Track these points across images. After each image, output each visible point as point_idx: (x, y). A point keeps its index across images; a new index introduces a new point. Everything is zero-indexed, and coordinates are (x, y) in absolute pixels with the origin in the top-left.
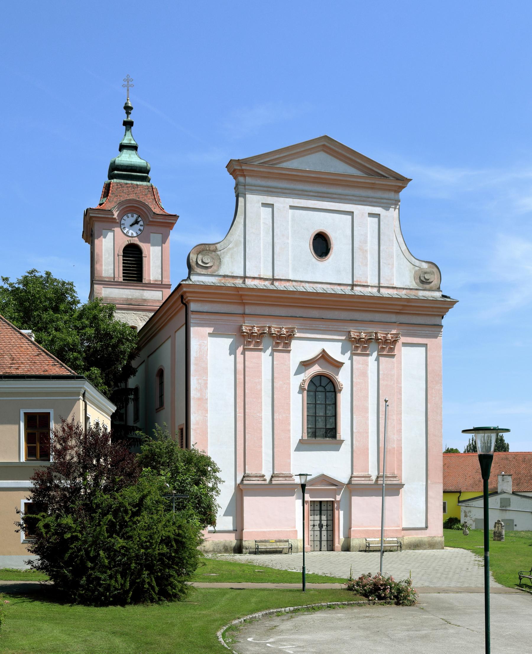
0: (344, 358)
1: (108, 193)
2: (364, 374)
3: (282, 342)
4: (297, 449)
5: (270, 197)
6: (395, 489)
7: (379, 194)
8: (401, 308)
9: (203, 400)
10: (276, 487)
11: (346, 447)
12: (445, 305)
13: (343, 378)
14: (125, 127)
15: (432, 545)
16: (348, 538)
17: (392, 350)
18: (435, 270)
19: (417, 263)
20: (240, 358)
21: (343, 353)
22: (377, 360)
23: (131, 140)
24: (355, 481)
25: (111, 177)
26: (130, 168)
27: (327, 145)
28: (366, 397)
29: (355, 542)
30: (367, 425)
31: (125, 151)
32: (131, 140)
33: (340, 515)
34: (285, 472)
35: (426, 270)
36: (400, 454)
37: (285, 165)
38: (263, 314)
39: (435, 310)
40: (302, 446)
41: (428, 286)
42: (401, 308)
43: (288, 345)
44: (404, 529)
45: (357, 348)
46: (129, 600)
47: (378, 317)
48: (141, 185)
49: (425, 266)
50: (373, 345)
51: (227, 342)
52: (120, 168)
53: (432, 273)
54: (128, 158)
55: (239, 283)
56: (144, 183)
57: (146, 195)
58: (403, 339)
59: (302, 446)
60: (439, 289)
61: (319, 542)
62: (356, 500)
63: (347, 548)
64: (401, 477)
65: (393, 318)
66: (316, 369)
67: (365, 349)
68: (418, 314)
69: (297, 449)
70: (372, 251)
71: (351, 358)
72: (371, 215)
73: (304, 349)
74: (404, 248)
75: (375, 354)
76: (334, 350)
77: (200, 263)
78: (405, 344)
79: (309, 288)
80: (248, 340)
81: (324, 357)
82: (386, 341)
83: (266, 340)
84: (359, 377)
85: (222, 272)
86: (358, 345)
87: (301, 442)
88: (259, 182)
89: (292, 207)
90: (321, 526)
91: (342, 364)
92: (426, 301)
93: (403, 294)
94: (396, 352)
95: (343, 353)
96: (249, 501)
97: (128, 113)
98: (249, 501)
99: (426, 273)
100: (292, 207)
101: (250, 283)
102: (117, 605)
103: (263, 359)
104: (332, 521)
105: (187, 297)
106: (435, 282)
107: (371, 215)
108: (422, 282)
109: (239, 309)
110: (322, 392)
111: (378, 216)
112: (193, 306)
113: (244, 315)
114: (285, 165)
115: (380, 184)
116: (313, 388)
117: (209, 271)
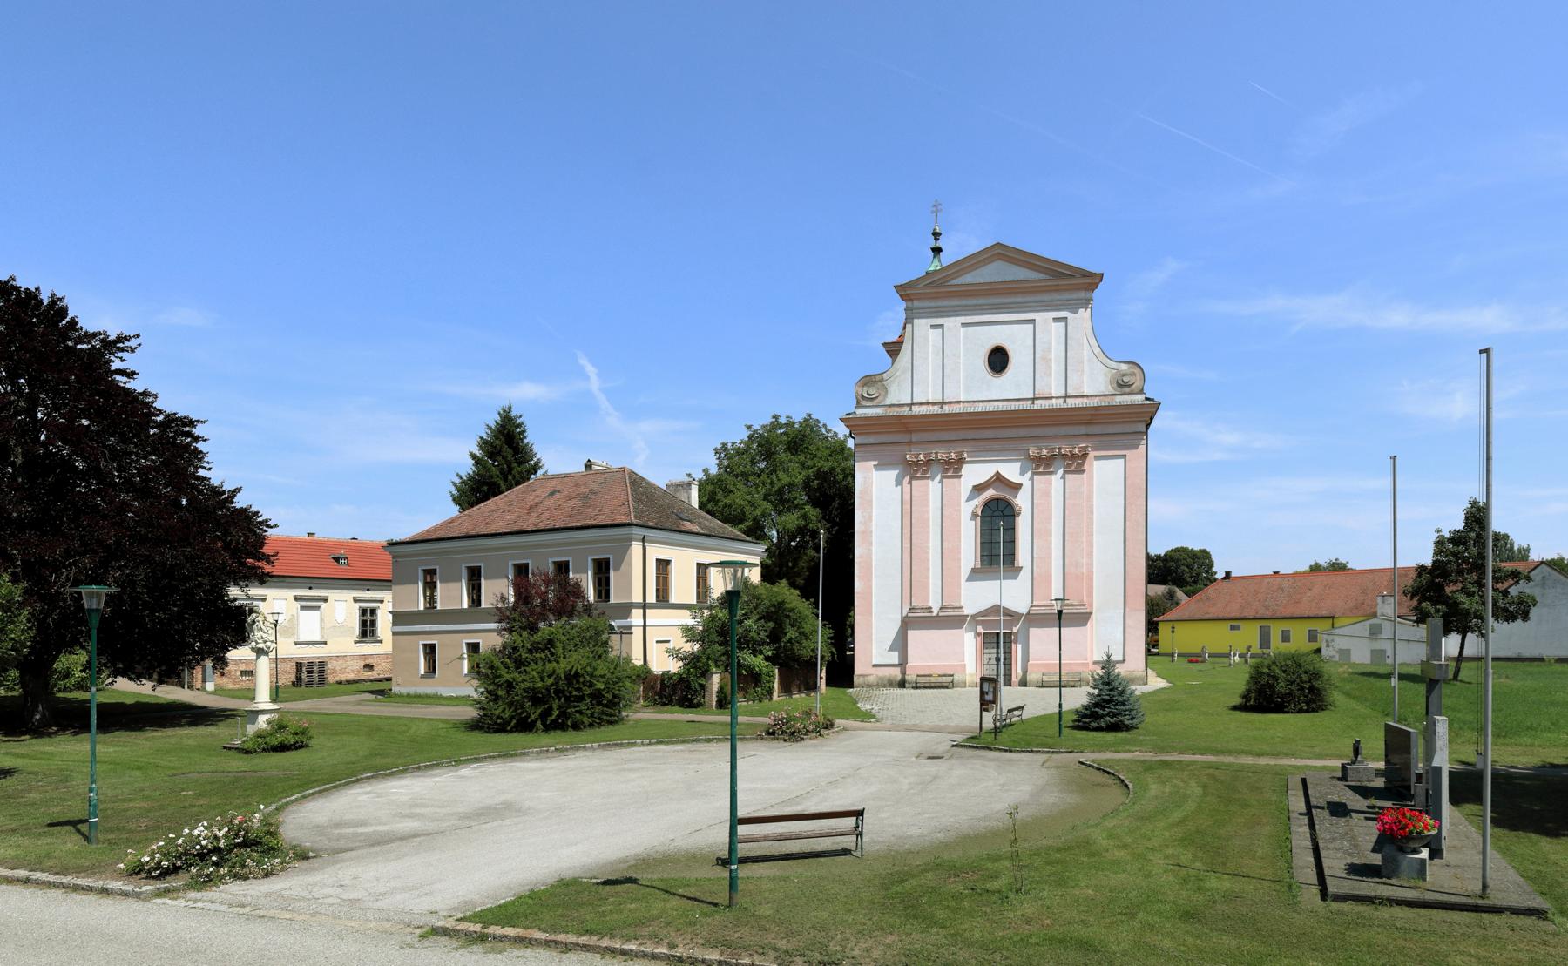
0: (1024, 480)
2: (1047, 494)
3: (953, 467)
4: (969, 579)
6: (1083, 619)
7: (1066, 296)
9: (867, 533)
10: (950, 620)
11: (1025, 575)
12: (1146, 415)
13: (1022, 501)
16: (1025, 672)
17: (1081, 465)
18: (1137, 370)
19: (1114, 365)
20: (907, 487)
21: (1022, 473)
22: (1063, 477)
24: (1035, 611)
27: (1000, 252)
28: (1049, 519)
29: (1031, 677)
30: (1049, 548)
33: (1018, 649)
34: (955, 603)
36: (1091, 579)
37: (955, 282)
38: (929, 441)
40: (975, 574)
43: (959, 469)
45: (1038, 466)
47: (1063, 430)
49: (1124, 367)
50: (1058, 462)
51: (892, 474)
53: (1133, 374)
55: (905, 411)
58: (1092, 454)
59: (975, 574)
60: (1141, 392)
62: (1034, 632)
63: (1023, 683)
64: (1091, 605)
65: (1083, 430)
66: (990, 493)
67: (1048, 466)
68: (1121, 423)
69: (969, 579)
70: (1059, 358)
71: (1032, 479)
72: (1056, 320)
73: (976, 472)
74: (1097, 350)
75: (1061, 472)
76: (1011, 470)
78: (1097, 458)
79: (980, 408)
80: (917, 469)
81: (998, 479)
82: (1072, 457)
83: (935, 468)
84: (1041, 499)
85: (888, 402)
86: (1041, 464)
87: (974, 570)
88: (927, 304)
89: (964, 325)
90: (998, 660)
91: (1020, 485)
92: (1132, 406)
93: (1092, 403)
94: (1086, 467)
95: (1022, 473)
96: (912, 635)
98: (912, 635)
100: (964, 325)
101: (917, 410)
102: (220, 499)
103: (932, 488)
104: (1008, 653)
106: (1138, 384)
107: (1056, 320)
108: (1120, 386)
109: (906, 438)
110: (998, 516)
111: (1065, 319)
113: (910, 443)
114: (955, 282)
115: (1065, 285)
116: (989, 512)
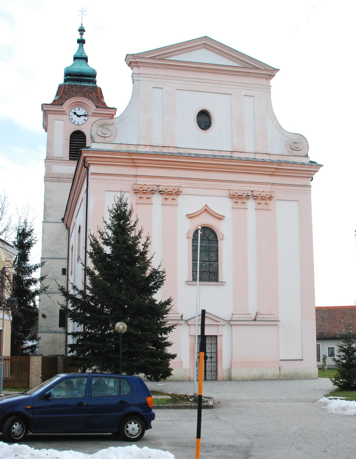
8: (273, 170)
13: (224, 230)
14: (78, 44)
15: (307, 377)
27: (206, 43)
35: (295, 141)
39: (303, 172)
41: (295, 153)
42: (273, 170)
44: (281, 360)
54: (80, 67)
56: (91, 85)
73: (189, 203)
97: (82, 34)
99: (295, 143)
105: (88, 161)
112: (92, 169)
117: (108, 140)
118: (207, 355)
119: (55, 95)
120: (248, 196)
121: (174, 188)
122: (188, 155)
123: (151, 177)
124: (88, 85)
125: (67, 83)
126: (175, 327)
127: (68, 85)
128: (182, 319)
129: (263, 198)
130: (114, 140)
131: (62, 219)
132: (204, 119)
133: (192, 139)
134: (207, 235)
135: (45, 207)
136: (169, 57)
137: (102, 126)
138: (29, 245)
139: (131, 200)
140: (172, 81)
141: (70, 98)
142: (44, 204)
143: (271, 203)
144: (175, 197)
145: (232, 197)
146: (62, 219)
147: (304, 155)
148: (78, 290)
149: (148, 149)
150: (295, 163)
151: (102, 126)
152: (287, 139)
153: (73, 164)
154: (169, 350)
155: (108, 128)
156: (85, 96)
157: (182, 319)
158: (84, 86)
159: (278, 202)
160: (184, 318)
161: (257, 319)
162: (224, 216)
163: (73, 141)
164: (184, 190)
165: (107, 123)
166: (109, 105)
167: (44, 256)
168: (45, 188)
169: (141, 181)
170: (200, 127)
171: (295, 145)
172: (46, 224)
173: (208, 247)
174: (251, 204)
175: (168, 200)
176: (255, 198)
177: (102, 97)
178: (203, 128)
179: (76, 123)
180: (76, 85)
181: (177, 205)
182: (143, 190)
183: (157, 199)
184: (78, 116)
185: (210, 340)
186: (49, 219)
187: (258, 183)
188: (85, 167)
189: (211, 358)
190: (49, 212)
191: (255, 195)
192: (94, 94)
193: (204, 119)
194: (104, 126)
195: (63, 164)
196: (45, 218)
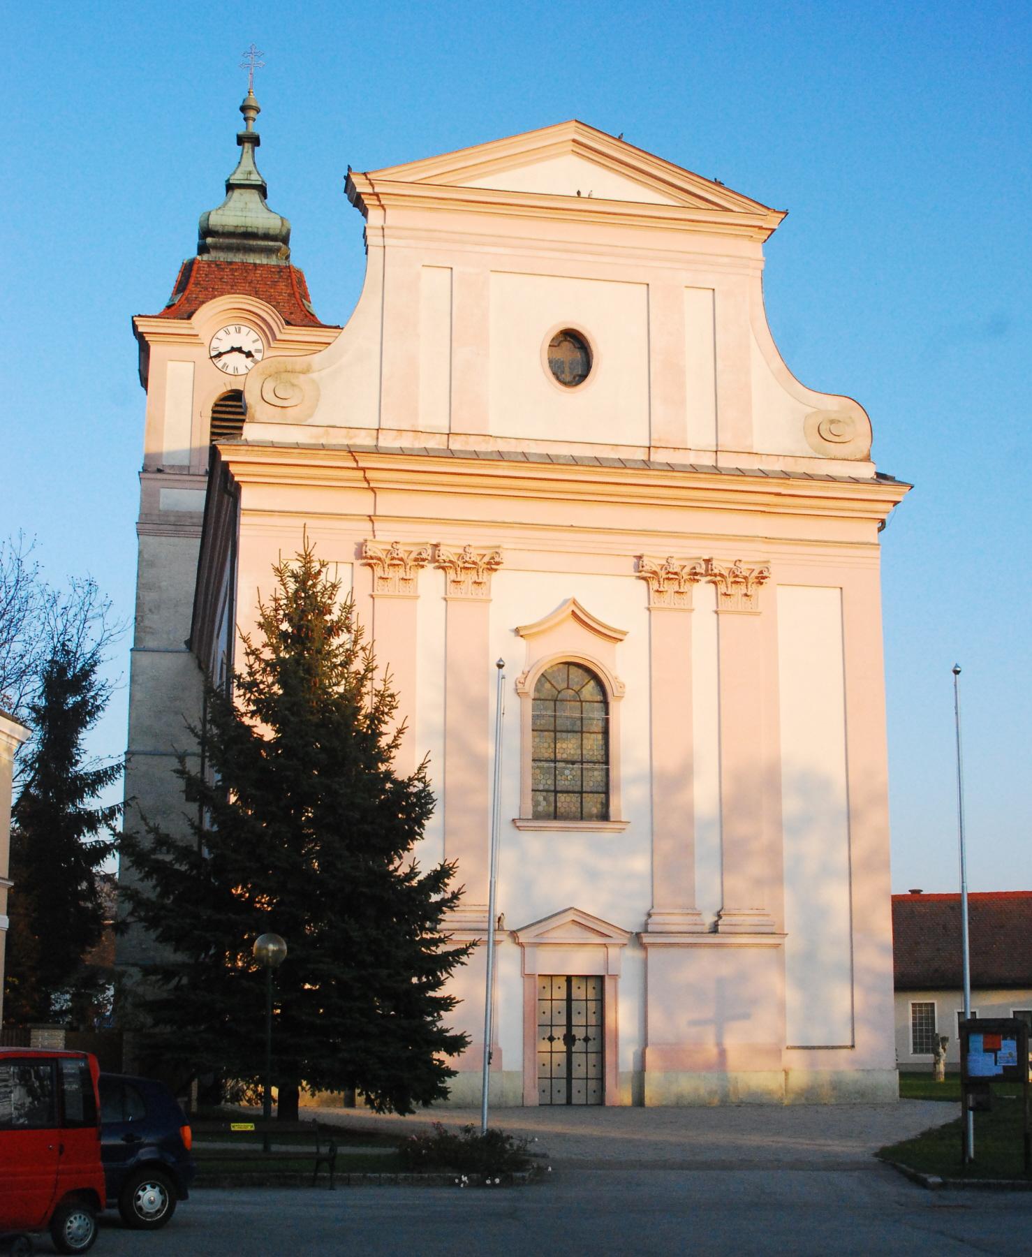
1: (187, 283)
5: (758, 297)
13: (624, 667)
23: (250, 173)
25: (203, 249)
26: (242, 230)
31: (237, 192)
32: (250, 173)
35: (834, 416)
41: (833, 449)
46: (10, 979)
48: (262, 265)
52: (220, 229)
54: (244, 212)
56: (273, 261)
57: (275, 283)
61: (574, 997)
77: (269, 396)
99: (832, 422)
118: (575, 1031)
119: (171, 289)
120: (696, 574)
121: (483, 552)
122: (521, 458)
123: (412, 516)
124: (265, 261)
125: (205, 257)
126: (470, 951)
127: (209, 263)
128: (500, 929)
129: (737, 579)
130: (310, 416)
131: (186, 643)
132: (573, 355)
133: (530, 411)
134: (577, 688)
135: (139, 606)
136: (466, 179)
137: (276, 374)
138: (83, 714)
139: (345, 582)
140: (478, 249)
141: (215, 297)
142: (138, 598)
143: (761, 592)
144: (484, 577)
145: (646, 576)
146: (186, 643)
147: (858, 457)
148: (176, 848)
149: (406, 442)
150: (832, 479)
151: (276, 374)
152: (809, 410)
153: (198, 485)
154: (449, 1022)
155: (294, 381)
156: (256, 294)
157: (500, 929)
158: (255, 264)
159: (780, 590)
160: (508, 925)
161: (650, 929)
162: (625, 633)
163: (217, 423)
164: (507, 557)
165: (289, 368)
166: (322, 319)
167: (134, 748)
168: (140, 553)
169: (386, 535)
170: (558, 378)
171: (833, 427)
172: (138, 655)
173: (579, 723)
174: (703, 593)
175: (463, 586)
176: (715, 579)
177: (306, 296)
178: (568, 379)
179: (230, 371)
180: (231, 263)
181: (417, 597)
182: (393, 559)
183: (430, 580)
184: (239, 350)
185: (583, 987)
186: (150, 643)
187: (725, 534)
188: (230, 494)
189: (586, 1040)
190: (152, 620)
191: (716, 571)
192: (282, 285)
193: (573, 355)
194: (284, 375)
195: (192, 485)
196: (137, 640)
